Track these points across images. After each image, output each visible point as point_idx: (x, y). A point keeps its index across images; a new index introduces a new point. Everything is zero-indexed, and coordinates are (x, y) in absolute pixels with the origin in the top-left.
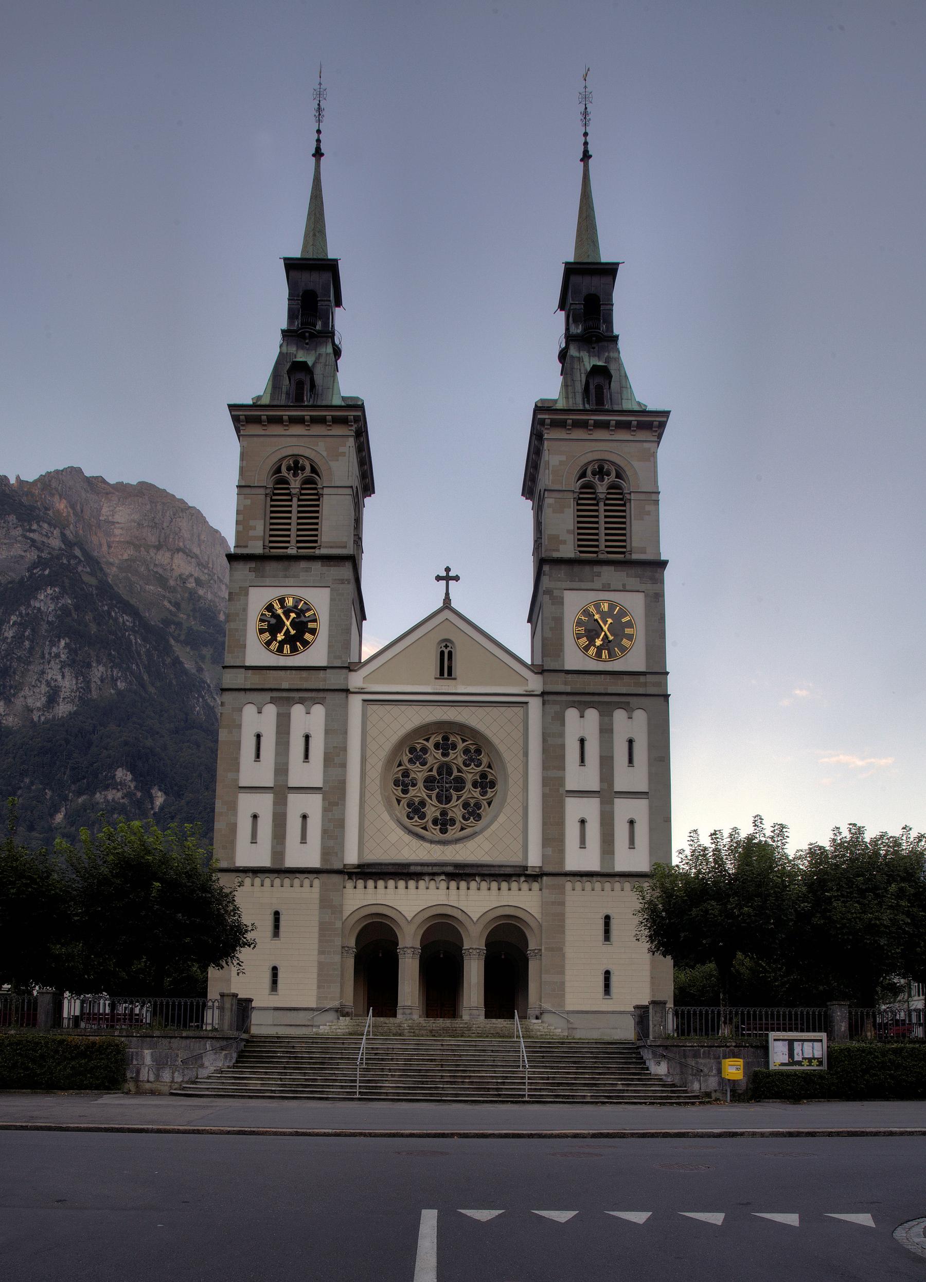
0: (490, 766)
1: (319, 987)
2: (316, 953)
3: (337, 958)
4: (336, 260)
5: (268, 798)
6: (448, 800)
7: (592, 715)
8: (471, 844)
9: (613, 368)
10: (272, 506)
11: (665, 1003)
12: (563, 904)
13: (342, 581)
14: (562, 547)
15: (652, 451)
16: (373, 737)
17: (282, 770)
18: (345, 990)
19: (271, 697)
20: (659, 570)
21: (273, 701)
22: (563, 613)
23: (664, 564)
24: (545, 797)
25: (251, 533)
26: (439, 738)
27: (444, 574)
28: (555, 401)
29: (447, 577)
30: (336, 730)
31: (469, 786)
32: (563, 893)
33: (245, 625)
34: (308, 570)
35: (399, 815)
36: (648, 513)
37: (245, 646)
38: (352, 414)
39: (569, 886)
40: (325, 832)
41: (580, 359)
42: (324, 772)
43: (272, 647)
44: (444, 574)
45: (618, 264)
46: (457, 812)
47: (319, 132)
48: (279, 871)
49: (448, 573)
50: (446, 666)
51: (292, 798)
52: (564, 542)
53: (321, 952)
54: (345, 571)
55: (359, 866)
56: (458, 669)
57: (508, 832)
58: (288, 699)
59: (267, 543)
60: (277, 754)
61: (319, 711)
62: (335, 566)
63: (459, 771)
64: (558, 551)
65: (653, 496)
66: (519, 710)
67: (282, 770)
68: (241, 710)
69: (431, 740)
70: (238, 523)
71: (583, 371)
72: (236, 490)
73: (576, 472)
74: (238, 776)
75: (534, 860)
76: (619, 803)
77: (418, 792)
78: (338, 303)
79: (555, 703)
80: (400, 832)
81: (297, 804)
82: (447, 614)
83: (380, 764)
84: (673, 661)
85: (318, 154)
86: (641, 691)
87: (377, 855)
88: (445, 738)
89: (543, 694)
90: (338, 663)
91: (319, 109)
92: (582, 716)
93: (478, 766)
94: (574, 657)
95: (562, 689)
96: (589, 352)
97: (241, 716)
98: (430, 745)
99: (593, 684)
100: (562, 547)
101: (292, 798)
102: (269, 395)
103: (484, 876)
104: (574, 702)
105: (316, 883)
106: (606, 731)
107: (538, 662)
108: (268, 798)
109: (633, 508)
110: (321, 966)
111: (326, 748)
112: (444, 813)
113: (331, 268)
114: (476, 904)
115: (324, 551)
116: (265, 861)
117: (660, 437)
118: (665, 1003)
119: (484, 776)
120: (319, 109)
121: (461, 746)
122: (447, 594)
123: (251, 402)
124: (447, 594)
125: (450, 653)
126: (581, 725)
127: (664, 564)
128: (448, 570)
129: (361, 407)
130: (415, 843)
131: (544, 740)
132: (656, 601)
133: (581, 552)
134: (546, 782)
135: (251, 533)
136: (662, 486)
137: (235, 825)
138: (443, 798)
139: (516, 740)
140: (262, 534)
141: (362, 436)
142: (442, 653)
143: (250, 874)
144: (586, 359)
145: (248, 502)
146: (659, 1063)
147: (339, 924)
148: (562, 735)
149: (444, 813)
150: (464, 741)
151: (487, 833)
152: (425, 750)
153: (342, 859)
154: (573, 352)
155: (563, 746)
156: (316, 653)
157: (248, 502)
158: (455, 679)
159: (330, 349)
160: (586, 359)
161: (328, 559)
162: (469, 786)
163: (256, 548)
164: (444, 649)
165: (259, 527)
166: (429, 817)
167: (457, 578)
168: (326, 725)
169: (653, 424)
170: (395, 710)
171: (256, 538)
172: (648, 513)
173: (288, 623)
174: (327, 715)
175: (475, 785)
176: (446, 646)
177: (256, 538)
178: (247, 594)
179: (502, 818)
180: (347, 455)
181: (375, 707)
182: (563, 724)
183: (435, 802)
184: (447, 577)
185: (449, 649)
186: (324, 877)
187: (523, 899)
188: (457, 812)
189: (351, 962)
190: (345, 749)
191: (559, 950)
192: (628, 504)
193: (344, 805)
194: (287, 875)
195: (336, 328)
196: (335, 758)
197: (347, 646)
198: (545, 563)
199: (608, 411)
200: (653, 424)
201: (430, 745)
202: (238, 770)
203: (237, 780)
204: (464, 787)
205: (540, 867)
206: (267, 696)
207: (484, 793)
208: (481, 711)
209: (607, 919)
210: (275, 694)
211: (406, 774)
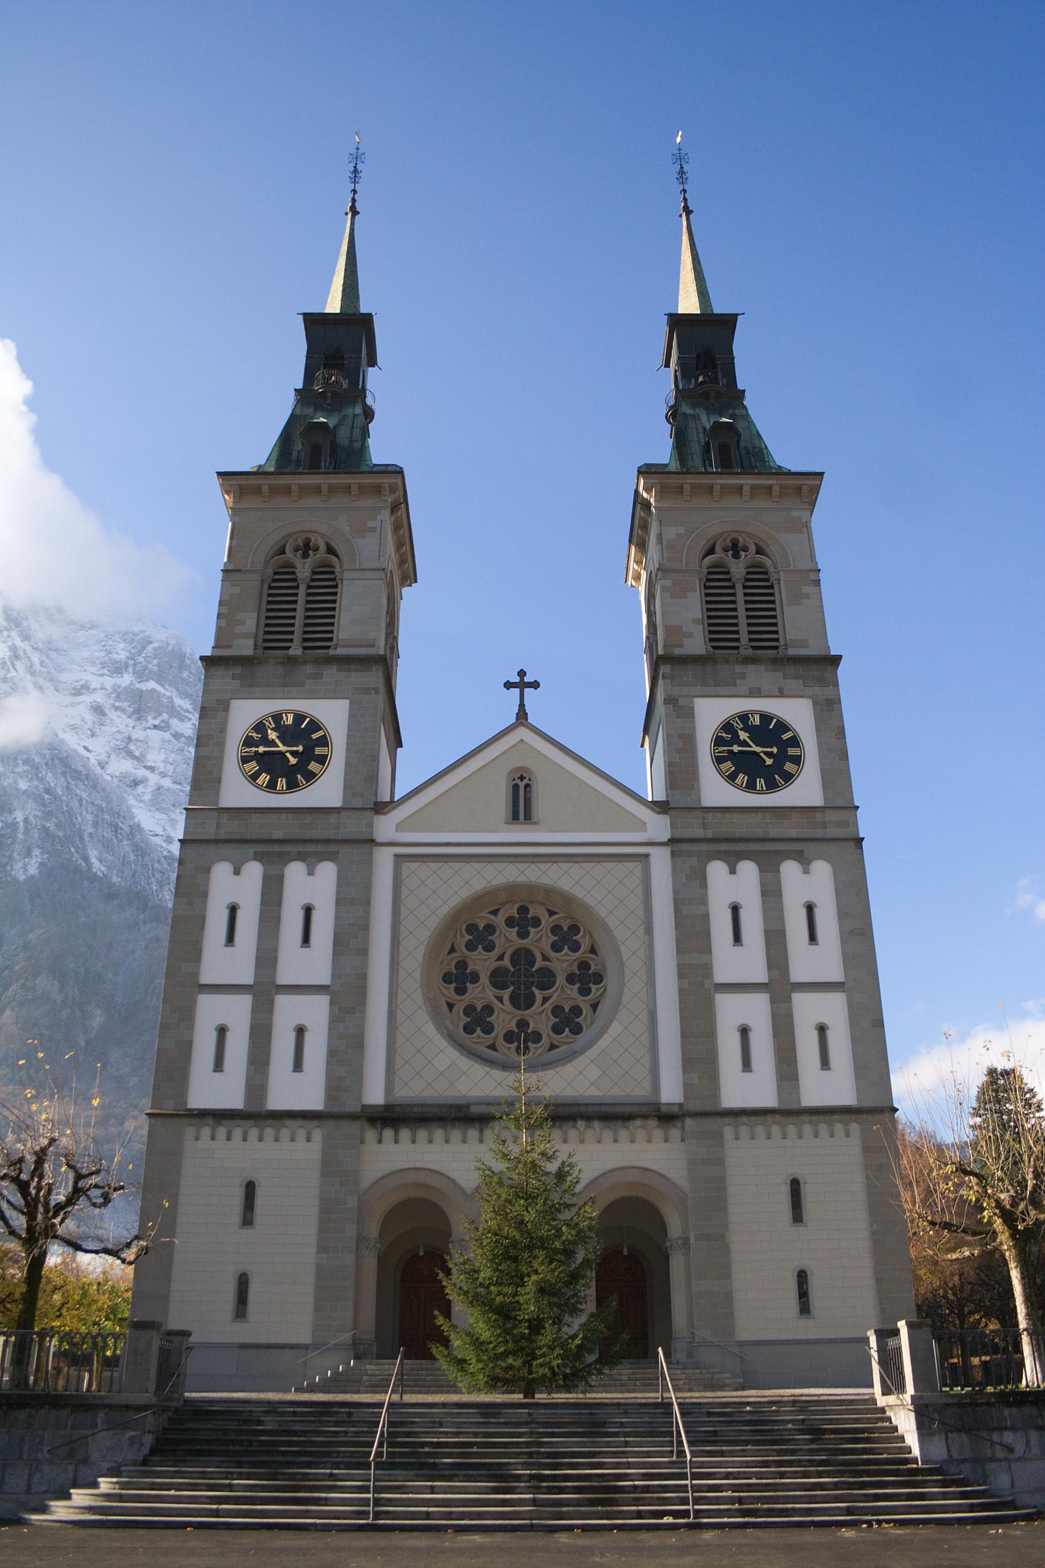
0: (593, 950)
1: (318, 1308)
2: (314, 1249)
3: (350, 1259)
4: (370, 315)
5: (245, 1001)
6: (530, 1002)
7: (748, 869)
8: (568, 1070)
9: (741, 425)
10: (270, 595)
12: (720, 1162)
13: (367, 691)
14: (686, 641)
15: (804, 520)
16: (409, 915)
17: (267, 958)
18: (362, 1308)
19: (256, 853)
20: (829, 668)
22: (693, 729)
23: (836, 660)
24: (683, 994)
25: (238, 629)
27: (517, 679)
28: (666, 465)
29: (522, 684)
30: (353, 899)
31: (561, 980)
32: (721, 1145)
33: (222, 751)
34: (317, 676)
35: (451, 1028)
36: (807, 596)
37: (219, 780)
38: (386, 481)
39: (728, 1132)
40: (333, 1055)
41: (696, 418)
42: (334, 961)
43: (260, 781)
44: (517, 679)
45: (736, 315)
47: (355, 191)
48: (256, 1116)
49: (522, 679)
50: (521, 803)
51: (282, 1001)
52: (690, 635)
53: (321, 1249)
54: (374, 678)
55: (388, 1107)
56: (541, 806)
57: (628, 1051)
58: (280, 854)
59: (260, 641)
60: (261, 936)
61: (328, 871)
62: (356, 671)
63: (545, 958)
64: (682, 646)
65: (812, 576)
66: (636, 867)
67: (267, 958)
68: (208, 870)
70: (220, 616)
71: (700, 430)
72: (220, 575)
73: (701, 548)
74: (199, 968)
75: (671, 1093)
76: (800, 1000)
77: (481, 993)
78: (373, 362)
79: (690, 854)
80: (453, 1054)
81: (289, 1011)
82: (522, 733)
83: (422, 949)
84: (863, 792)
85: (355, 212)
86: (819, 833)
87: (418, 1088)
89: (672, 841)
90: (358, 803)
91: (355, 171)
92: (733, 871)
93: (575, 951)
94: (239, 790)
95: (700, 840)
96: (706, 408)
97: (208, 879)
98: (500, 920)
99: (743, 827)
100: (686, 641)
101: (282, 1001)
102: (273, 462)
103: (588, 1118)
104: (719, 852)
105: (317, 1134)
106: (771, 894)
107: (661, 797)
108: (245, 1001)
109: (783, 593)
110: (321, 1272)
111: (336, 926)
112: (522, 1024)
113: (367, 321)
115: (340, 651)
116: (236, 1101)
117: (813, 504)
119: (584, 965)
120: (355, 171)
122: (522, 705)
123: (255, 470)
124: (522, 705)
125: (527, 786)
126: (731, 885)
127: (836, 660)
128: (522, 673)
129: (399, 472)
130: (478, 1070)
131: (677, 910)
132: (829, 711)
133: (714, 648)
134: (683, 971)
135: (238, 629)
136: (823, 559)
137: (190, 1044)
138: (522, 1001)
139: (636, 916)
140: (253, 630)
141: (400, 505)
142: (516, 787)
143: (211, 1121)
144: (704, 418)
145: (237, 590)
147: (352, 1202)
148: (704, 901)
149: (522, 1024)
150: (551, 913)
151: (592, 1053)
152: (490, 929)
153: (359, 1097)
154: (686, 409)
155: (706, 918)
156: (326, 790)
157: (237, 590)
158: (536, 823)
159: (358, 410)
160: (704, 418)
161: (347, 662)
163: (245, 647)
164: (518, 781)
165: (250, 622)
166: (500, 1030)
167: (535, 685)
168: (338, 892)
169: (805, 487)
170: (445, 870)
171: (245, 636)
172: (807, 596)
173: (282, 748)
174: (339, 878)
175: (571, 979)
176: (522, 778)
177: (245, 636)
178: (227, 709)
179: (615, 1029)
180: (378, 530)
181: (414, 866)
182: (704, 885)
183: (507, 1005)
184: (522, 684)
185: (525, 781)
186: (330, 1124)
189: (371, 1263)
190: (366, 927)
191: (718, 1239)
192: (776, 586)
193: (363, 1011)
194: (270, 1122)
195: (369, 386)
196: (351, 941)
197: (373, 777)
198: (664, 662)
200: (805, 487)
201: (500, 920)
202: (198, 960)
203: (196, 975)
204: (554, 984)
205: (680, 1105)
206: (251, 849)
208: (576, 870)
209: (795, 1185)
210: (261, 848)
211: (462, 965)
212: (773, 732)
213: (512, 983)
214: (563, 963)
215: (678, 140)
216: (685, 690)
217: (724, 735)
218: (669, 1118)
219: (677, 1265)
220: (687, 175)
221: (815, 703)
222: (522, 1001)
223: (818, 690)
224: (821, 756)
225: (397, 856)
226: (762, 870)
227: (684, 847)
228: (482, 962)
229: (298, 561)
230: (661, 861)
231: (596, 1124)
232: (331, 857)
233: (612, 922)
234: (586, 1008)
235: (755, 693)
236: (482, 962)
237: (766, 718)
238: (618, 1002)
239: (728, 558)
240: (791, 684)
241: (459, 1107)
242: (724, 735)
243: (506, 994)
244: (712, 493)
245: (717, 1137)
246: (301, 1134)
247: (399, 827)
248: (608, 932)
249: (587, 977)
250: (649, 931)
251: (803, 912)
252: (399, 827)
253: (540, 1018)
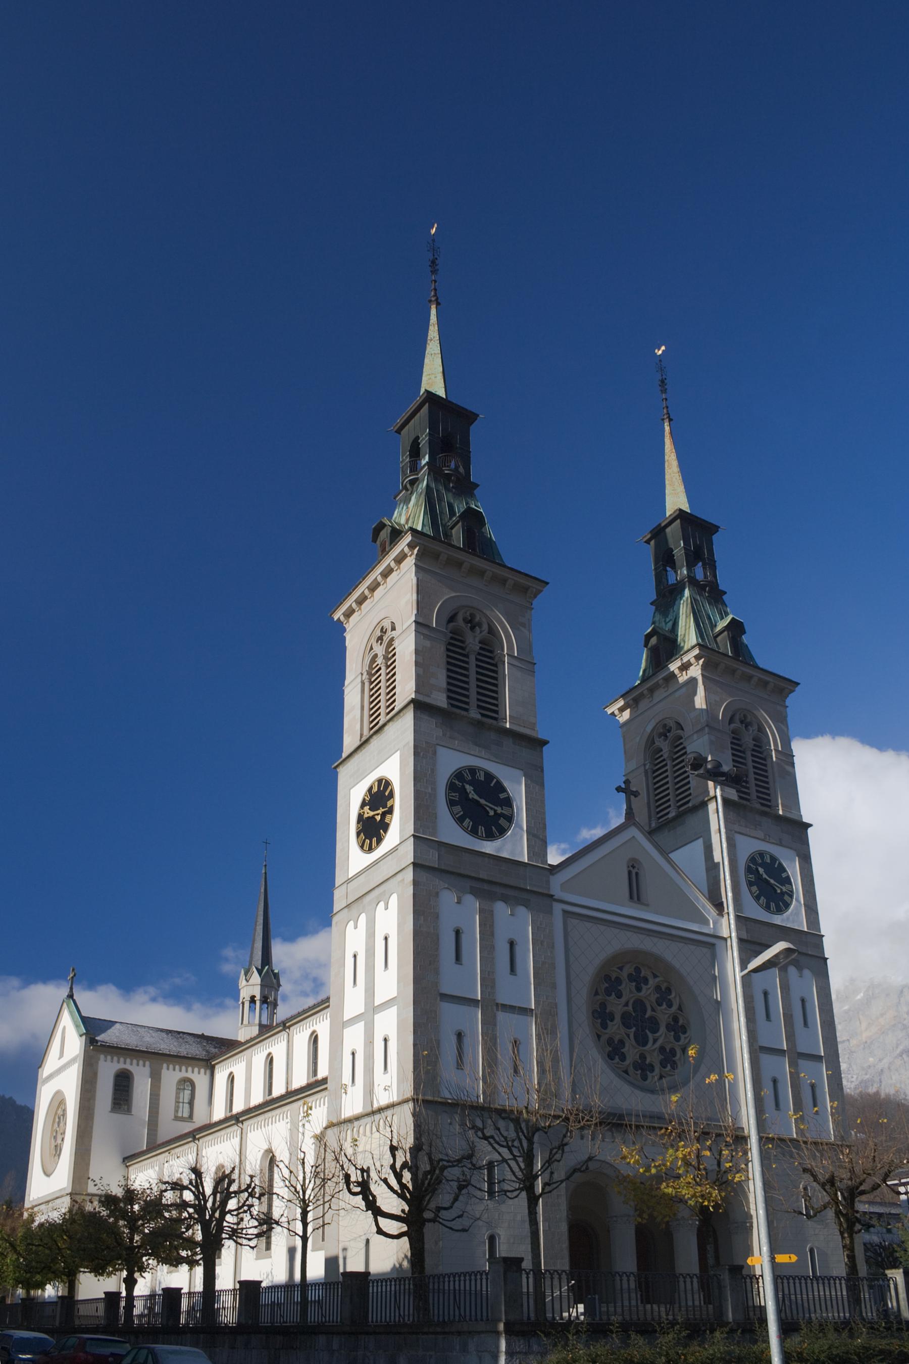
11: (522, 1260)
21: (475, 892)
26: (632, 971)
31: (663, 1029)
46: (654, 1058)
63: (653, 1010)
69: (657, 980)
88: (638, 970)
112: (643, 1057)
118: (522, 1260)
121: (652, 982)
125: (637, 874)
142: (630, 873)
146: (43, 1290)
156: (515, 845)
162: (663, 1029)
188: (654, 1058)
199: (689, 650)
207: (677, 1039)
211: (603, 1005)
212: (494, 790)
213: (635, 1025)
215: (433, 231)
217: (457, 782)
220: (437, 267)
232: (526, 904)
236: (617, 1007)
237: (489, 776)
239: (466, 628)
242: (457, 782)
244: (505, 585)
251: (453, 935)
252: (564, 886)
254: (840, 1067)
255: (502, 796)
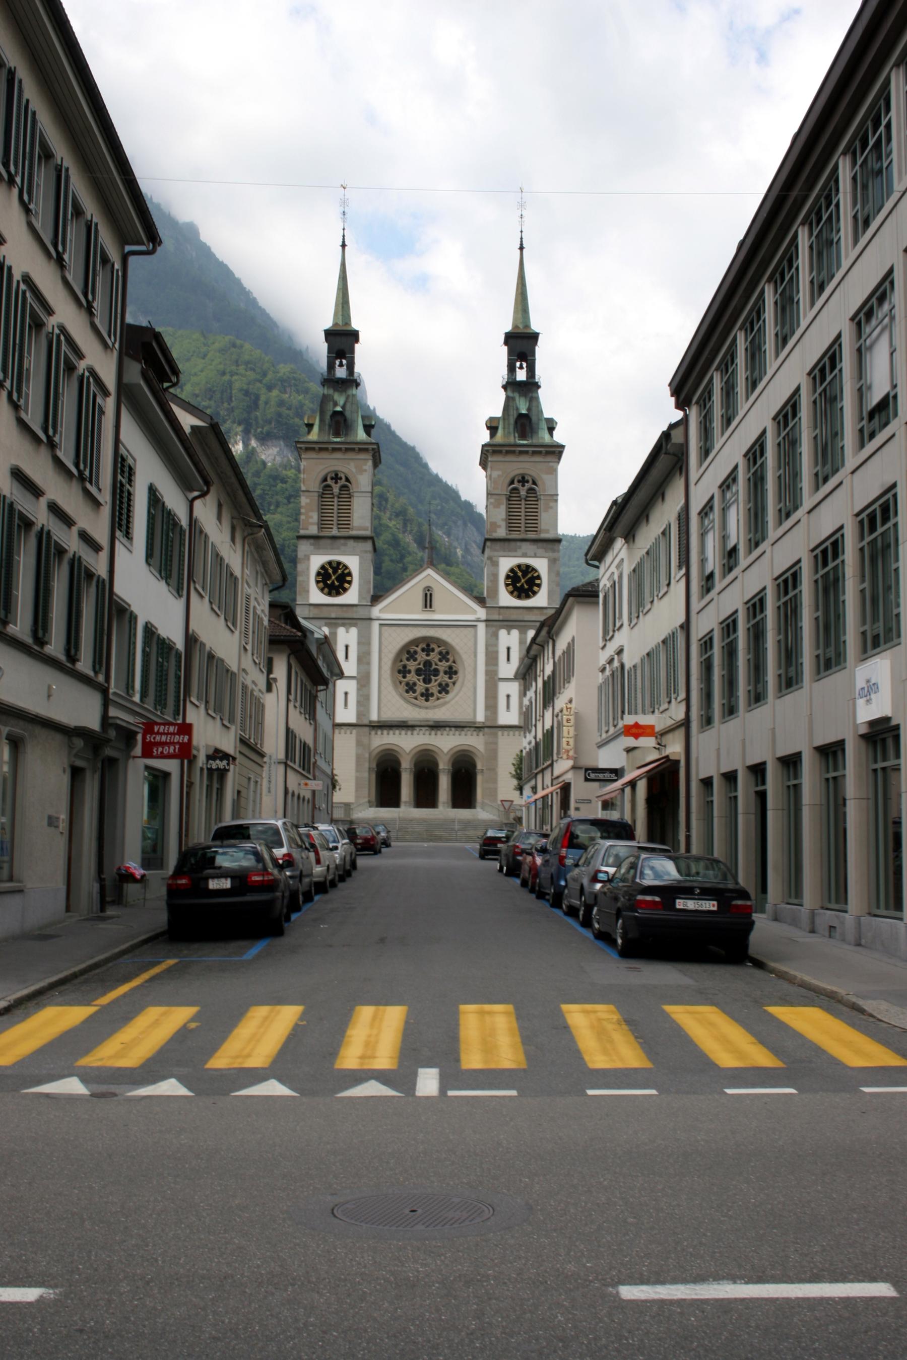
0: (454, 662)
6: (429, 681)
8: (443, 709)
12: (496, 743)
25: (311, 520)
30: (364, 642)
31: (442, 674)
34: (345, 545)
36: (551, 508)
53: (357, 771)
55: (378, 722)
61: (354, 631)
65: (554, 497)
73: (508, 480)
75: (480, 717)
79: (493, 626)
89: (486, 621)
99: (514, 615)
103: (450, 727)
105: (354, 732)
110: (357, 778)
112: (427, 690)
114: (445, 744)
115: (354, 533)
119: (450, 667)
125: (431, 595)
131: (487, 649)
135: (311, 520)
138: (427, 681)
142: (426, 595)
166: (418, 693)
175: (445, 673)
177: (313, 524)
178: (309, 559)
186: (358, 729)
187: (474, 742)
208: (449, 631)
211: (405, 666)
214: (443, 666)
216: (496, 554)
218: (478, 728)
219: (479, 779)
221: (549, 560)
222: (427, 681)
223: (550, 554)
224: (549, 585)
225: (381, 625)
226: (520, 633)
227: (491, 623)
228: (412, 666)
229: (333, 485)
230: (481, 627)
231: (453, 729)
232: (355, 625)
233: (461, 652)
234: (451, 685)
235: (525, 555)
236: (412, 666)
238: (463, 683)
240: (540, 551)
241: (404, 722)
243: (421, 678)
245: (496, 735)
246: (348, 732)
247: (381, 611)
248: (458, 653)
249: (451, 672)
250: (475, 656)
252: (381, 611)
253: (434, 687)
254: (475, 1071)
255: (322, 571)
